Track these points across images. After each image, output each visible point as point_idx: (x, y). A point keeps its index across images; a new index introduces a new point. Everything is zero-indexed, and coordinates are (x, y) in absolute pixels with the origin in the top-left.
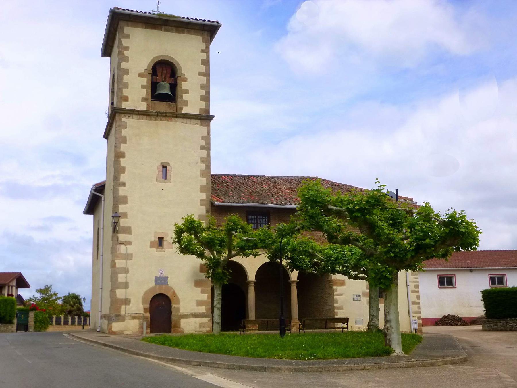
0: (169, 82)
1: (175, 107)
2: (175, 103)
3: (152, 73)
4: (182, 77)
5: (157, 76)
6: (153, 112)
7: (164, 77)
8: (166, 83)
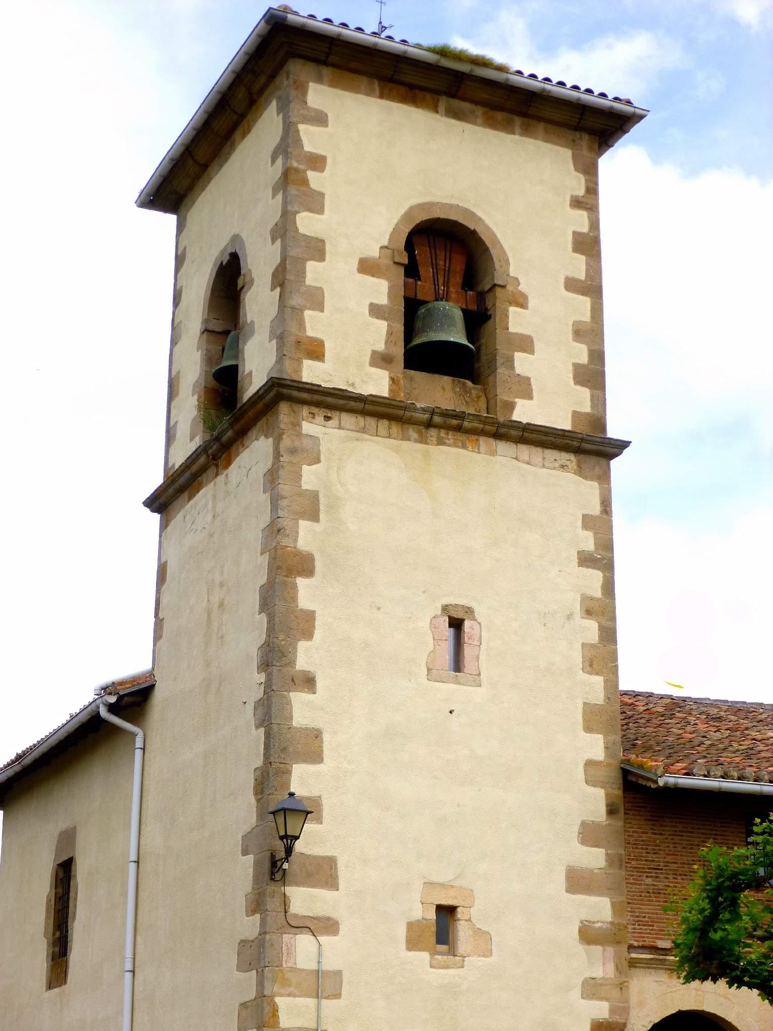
4: (509, 288)
7: (441, 281)
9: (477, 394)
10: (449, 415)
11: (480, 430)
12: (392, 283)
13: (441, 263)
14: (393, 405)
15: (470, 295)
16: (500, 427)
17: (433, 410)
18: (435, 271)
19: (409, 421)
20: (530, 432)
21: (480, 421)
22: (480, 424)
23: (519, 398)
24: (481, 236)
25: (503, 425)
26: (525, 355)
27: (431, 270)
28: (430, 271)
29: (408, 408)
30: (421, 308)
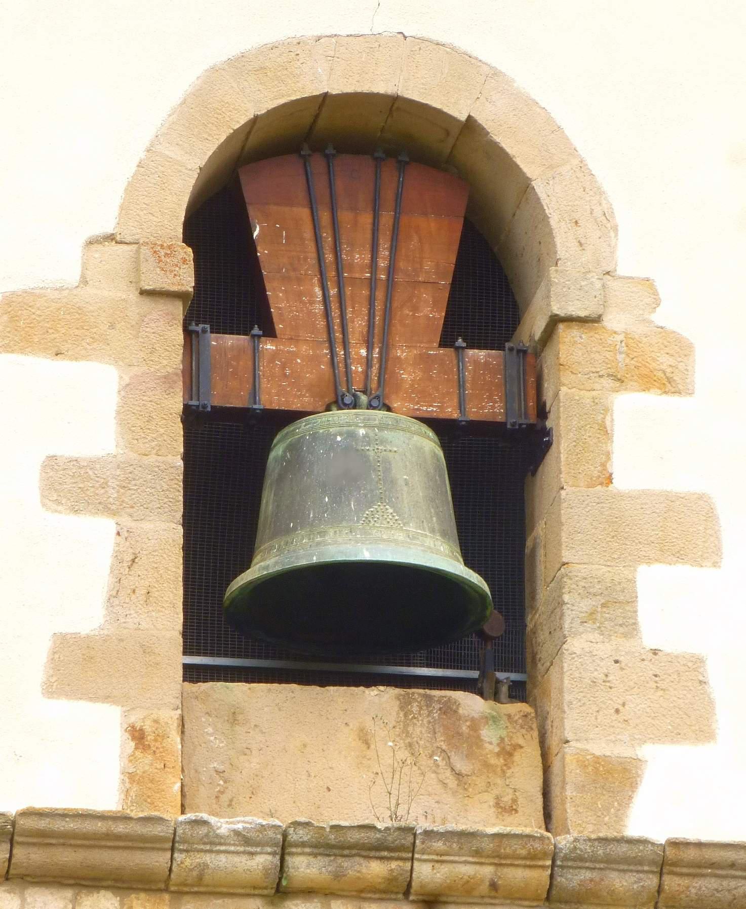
0: (432, 410)
1: (530, 755)
2: (519, 692)
3: (186, 280)
4: (614, 321)
5: (270, 332)
6: (213, 842)
7: (358, 325)
8: (382, 427)
9: (502, 739)
10: (350, 847)
11: (484, 888)
12: (135, 370)
13: (359, 257)
14: (118, 837)
15: (476, 363)
16: (562, 867)
17: (285, 835)
18: (333, 292)
19: (199, 885)
20: (692, 871)
21: (477, 853)
22: (481, 864)
23: (659, 738)
24: (497, 139)
25: (574, 860)
26: (682, 572)
27: (318, 291)
28: (312, 295)
29: (184, 841)
30: (278, 437)
